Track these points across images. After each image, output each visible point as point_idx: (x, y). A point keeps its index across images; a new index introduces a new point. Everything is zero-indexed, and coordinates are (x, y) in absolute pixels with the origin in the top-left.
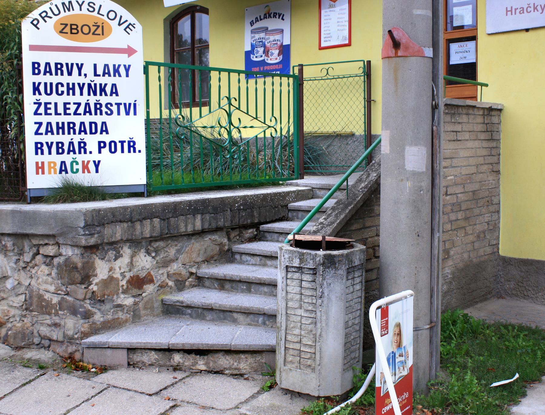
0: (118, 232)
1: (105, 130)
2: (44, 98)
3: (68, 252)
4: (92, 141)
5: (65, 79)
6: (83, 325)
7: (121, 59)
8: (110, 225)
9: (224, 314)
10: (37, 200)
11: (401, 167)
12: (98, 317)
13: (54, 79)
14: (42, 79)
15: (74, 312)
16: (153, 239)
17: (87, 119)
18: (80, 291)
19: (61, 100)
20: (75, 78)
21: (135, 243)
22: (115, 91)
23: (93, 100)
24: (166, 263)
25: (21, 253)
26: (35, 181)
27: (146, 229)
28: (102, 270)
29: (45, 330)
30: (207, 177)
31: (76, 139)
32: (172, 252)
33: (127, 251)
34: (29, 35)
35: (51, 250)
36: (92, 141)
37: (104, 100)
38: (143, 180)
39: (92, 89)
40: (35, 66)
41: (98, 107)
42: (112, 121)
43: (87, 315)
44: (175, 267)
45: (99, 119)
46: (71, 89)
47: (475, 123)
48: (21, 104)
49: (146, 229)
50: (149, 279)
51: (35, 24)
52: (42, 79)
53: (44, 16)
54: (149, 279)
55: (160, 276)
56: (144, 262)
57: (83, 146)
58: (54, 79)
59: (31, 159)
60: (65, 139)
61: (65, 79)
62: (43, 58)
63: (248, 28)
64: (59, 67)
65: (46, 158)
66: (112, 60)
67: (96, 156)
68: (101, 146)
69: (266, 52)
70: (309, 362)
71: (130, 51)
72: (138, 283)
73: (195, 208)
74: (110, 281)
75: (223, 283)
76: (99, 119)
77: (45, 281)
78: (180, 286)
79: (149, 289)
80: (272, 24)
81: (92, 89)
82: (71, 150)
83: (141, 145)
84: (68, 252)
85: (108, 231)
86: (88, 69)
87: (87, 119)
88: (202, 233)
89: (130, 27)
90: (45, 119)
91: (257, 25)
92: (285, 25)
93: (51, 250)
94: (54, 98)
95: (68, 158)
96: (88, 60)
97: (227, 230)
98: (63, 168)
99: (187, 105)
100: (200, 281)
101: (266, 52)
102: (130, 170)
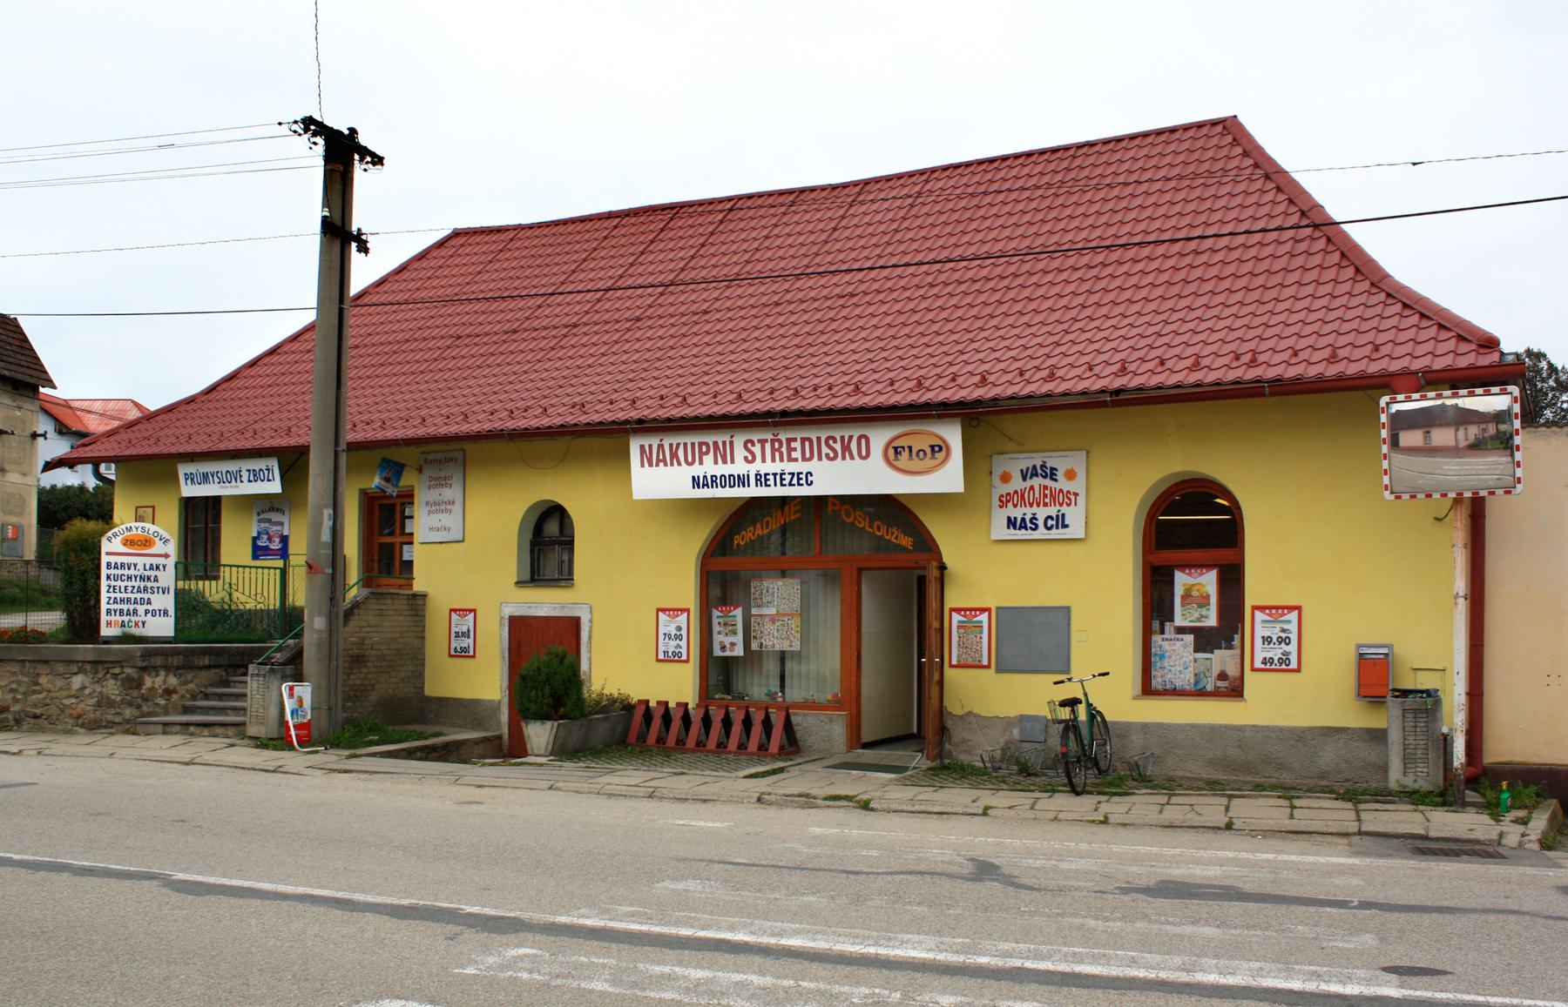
0: (159, 661)
1: (149, 602)
2: (113, 583)
3: (128, 670)
4: (141, 609)
5: (126, 572)
6: (136, 712)
7: (161, 561)
8: (152, 654)
9: (221, 710)
10: (105, 643)
11: (312, 627)
12: (145, 709)
13: (120, 572)
14: (112, 571)
15: (130, 704)
16: (178, 668)
17: (139, 596)
18: (135, 693)
19: (123, 584)
20: (132, 572)
21: (168, 669)
22: (156, 580)
23: (142, 584)
24: (186, 683)
25: (96, 673)
26: (105, 631)
27: (175, 661)
28: (148, 682)
29: (110, 717)
30: (214, 636)
31: (132, 607)
32: (190, 676)
33: (162, 673)
34: (106, 546)
35: (117, 671)
36: (141, 609)
37: (149, 585)
38: (172, 634)
39: (142, 578)
40: (109, 565)
41: (146, 589)
42: (154, 597)
43: (139, 707)
44: (191, 686)
45: (146, 596)
46: (129, 578)
47: (401, 604)
48: (99, 586)
49: (175, 661)
50: (174, 691)
51: (109, 540)
52: (112, 571)
53: (115, 535)
54: (174, 691)
55: (182, 690)
56: (173, 681)
57: (135, 612)
58: (120, 572)
59: (104, 618)
60: (125, 607)
61: (126, 572)
62: (113, 559)
63: (256, 518)
64: (123, 565)
65: (112, 618)
66: (155, 561)
67: (143, 618)
68: (147, 612)
69: (270, 539)
70: (261, 721)
71: (166, 556)
72: (168, 692)
73: (204, 652)
74: (152, 689)
75: (220, 697)
76: (146, 596)
77: (112, 688)
78: (194, 698)
79: (175, 697)
80: (276, 517)
81: (142, 578)
82: (128, 614)
83: (172, 612)
84: (128, 670)
85: (153, 660)
86: (140, 566)
87: (139, 596)
88: (209, 667)
89: (167, 541)
90: (113, 595)
91: (263, 516)
92: (284, 519)
93: (117, 671)
94: (119, 583)
95: (126, 619)
96: (140, 561)
97: (227, 667)
98: (123, 625)
99: (201, 578)
100: (207, 696)
101: (270, 539)
102: (163, 627)
